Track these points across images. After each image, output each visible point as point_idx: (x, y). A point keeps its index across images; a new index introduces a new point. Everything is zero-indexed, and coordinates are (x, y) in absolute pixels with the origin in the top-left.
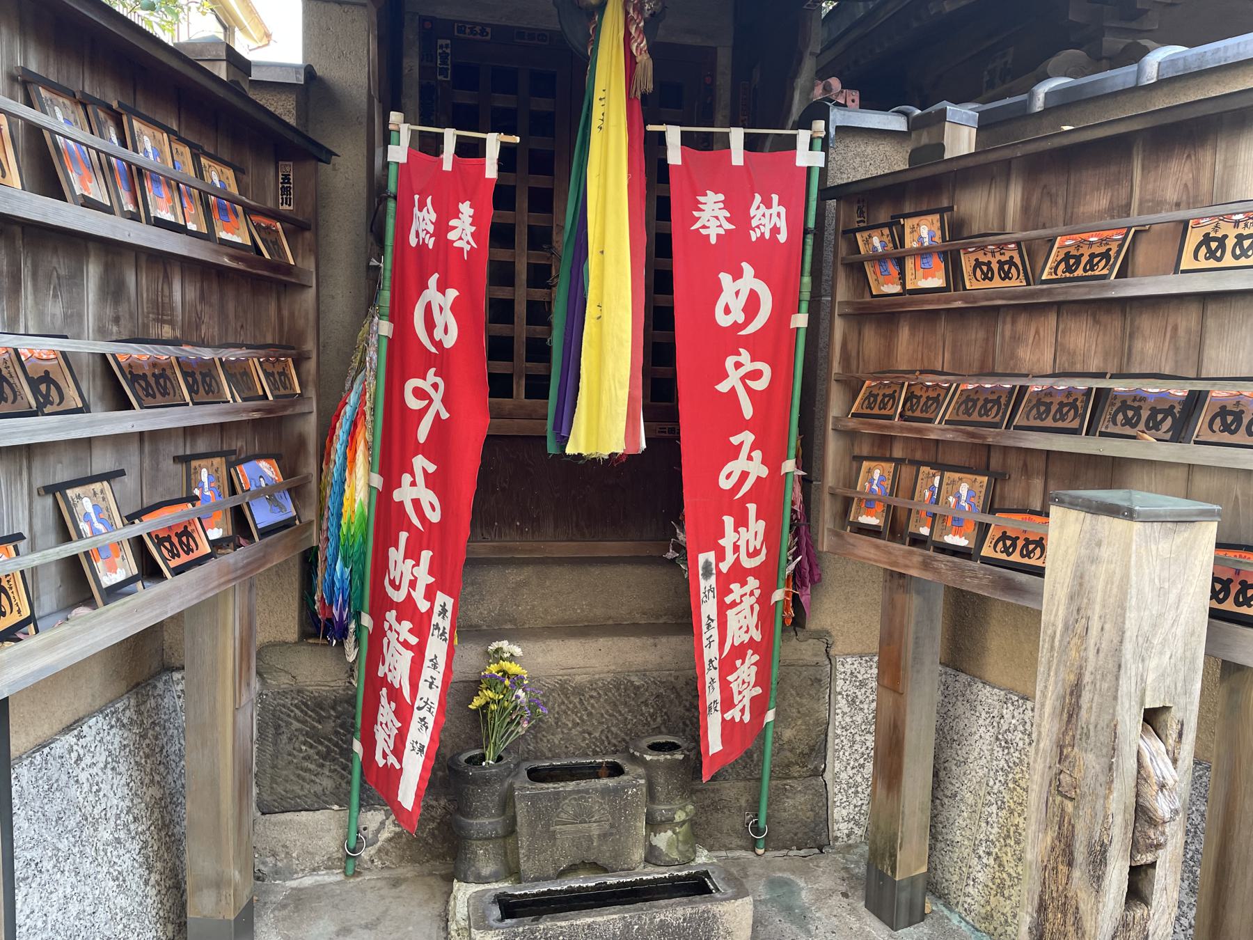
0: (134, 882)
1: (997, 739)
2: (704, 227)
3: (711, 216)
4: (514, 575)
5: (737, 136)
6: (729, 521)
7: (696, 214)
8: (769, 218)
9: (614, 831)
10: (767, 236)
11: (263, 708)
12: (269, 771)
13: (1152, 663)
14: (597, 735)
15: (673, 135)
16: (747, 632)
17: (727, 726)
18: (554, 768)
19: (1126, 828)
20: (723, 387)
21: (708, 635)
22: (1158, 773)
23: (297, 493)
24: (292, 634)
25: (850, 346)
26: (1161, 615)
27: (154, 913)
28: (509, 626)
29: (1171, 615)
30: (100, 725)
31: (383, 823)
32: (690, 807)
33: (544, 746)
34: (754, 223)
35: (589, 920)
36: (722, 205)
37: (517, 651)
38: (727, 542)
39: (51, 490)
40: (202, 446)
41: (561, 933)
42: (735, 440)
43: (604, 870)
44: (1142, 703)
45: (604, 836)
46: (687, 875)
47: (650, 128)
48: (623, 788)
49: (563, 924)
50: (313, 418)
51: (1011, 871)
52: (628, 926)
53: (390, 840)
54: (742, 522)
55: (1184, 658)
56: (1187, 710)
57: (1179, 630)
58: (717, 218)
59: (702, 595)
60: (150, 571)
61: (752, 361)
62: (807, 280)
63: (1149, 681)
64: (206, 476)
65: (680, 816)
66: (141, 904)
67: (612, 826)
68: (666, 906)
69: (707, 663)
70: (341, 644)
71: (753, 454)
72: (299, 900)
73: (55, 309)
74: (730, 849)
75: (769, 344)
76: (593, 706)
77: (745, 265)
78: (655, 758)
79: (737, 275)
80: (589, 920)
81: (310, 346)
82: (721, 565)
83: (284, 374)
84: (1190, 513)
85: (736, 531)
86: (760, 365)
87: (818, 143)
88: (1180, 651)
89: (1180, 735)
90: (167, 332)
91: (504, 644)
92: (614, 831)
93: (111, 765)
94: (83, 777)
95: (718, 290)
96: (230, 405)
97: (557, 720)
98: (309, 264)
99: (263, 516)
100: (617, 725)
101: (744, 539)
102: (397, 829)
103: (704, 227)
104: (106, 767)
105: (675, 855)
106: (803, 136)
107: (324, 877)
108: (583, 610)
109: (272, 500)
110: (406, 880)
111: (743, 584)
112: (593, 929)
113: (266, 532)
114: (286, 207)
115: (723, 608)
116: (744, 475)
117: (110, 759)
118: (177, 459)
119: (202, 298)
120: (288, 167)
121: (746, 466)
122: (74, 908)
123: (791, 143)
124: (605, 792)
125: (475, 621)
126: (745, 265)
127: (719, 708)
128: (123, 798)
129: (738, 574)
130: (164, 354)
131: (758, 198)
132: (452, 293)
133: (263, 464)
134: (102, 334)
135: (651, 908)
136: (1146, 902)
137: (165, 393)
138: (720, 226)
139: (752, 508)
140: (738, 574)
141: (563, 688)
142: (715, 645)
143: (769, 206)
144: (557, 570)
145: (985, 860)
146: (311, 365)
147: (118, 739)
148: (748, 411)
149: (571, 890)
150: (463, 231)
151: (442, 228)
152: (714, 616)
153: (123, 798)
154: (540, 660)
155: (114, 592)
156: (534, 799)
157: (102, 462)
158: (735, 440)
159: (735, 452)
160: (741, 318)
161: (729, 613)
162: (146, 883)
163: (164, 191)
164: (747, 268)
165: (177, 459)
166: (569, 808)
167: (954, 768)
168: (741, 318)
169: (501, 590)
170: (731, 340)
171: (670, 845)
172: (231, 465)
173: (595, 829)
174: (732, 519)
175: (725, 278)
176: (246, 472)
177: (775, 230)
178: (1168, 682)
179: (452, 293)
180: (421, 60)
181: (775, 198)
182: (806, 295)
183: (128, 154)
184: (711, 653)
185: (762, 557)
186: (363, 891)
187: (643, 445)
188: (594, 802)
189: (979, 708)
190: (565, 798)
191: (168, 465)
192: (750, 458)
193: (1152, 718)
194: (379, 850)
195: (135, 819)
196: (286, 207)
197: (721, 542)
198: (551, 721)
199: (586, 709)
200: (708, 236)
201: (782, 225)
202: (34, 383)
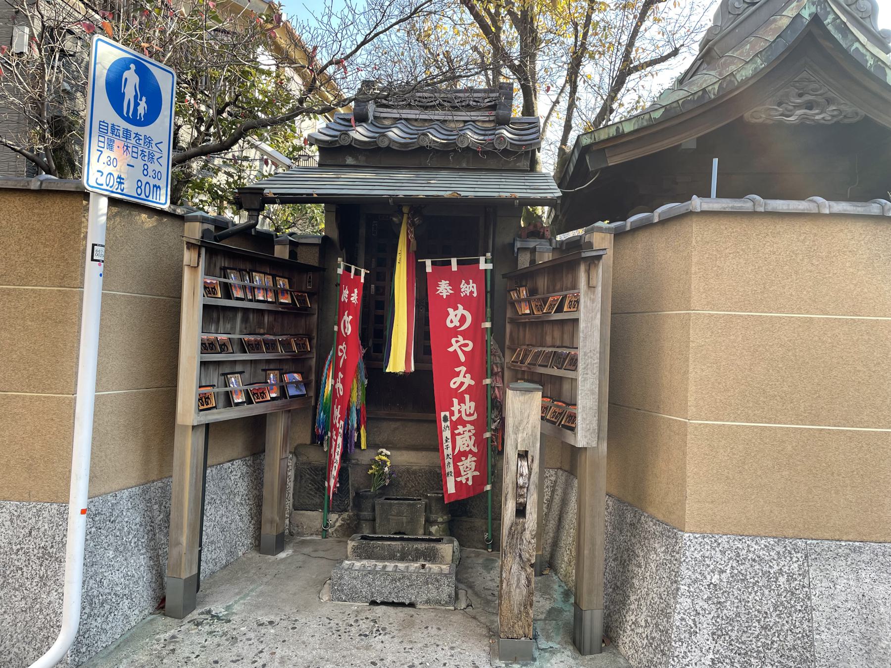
0: (246, 519)
3: (444, 289)
4: (394, 425)
5: (454, 261)
6: (455, 401)
8: (469, 288)
13: (520, 435)
15: (428, 262)
17: (458, 484)
20: (451, 349)
23: (307, 385)
24: (308, 442)
26: (522, 420)
29: (525, 421)
37: (389, 453)
38: (456, 408)
39: (223, 374)
40: (272, 367)
42: (457, 369)
43: (404, 534)
45: (408, 522)
50: (314, 360)
52: (403, 548)
53: (340, 526)
54: (462, 401)
56: (535, 451)
57: (530, 426)
60: (249, 401)
62: (489, 310)
64: (272, 377)
65: (440, 520)
70: (322, 444)
73: (228, 326)
75: (472, 333)
79: (456, 309)
81: (315, 334)
83: (304, 344)
86: (467, 342)
89: (533, 460)
90: (262, 331)
91: (384, 450)
93: (242, 477)
94: (232, 478)
95: (448, 314)
96: (281, 352)
98: (316, 306)
99: (292, 391)
101: (465, 408)
106: (482, 259)
107: (314, 537)
109: (297, 387)
111: (464, 426)
113: (291, 397)
115: (453, 436)
116: (462, 384)
118: (263, 370)
121: (463, 379)
122: (224, 519)
123: (478, 261)
129: (461, 422)
130: (259, 338)
132: (351, 317)
133: (296, 375)
134: (241, 333)
136: (524, 516)
137: (258, 349)
139: (467, 397)
140: (461, 422)
141: (408, 471)
142: (450, 449)
143: (468, 284)
146: (315, 341)
148: (463, 358)
150: (354, 298)
151: (349, 296)
152: (449, 437)
155: (237, 404)
156: (382, 504)
157: (239, 368)
158: (457, 369)
159: (458, 374)
160: (458, 324)
161: (457, 437)
163: (261, 291)
165: (263, 370)
168: (458, 324)
169: (387, 429)
170: (455, 332)
172: (281, 374)
173: (405, 519)
175: (450, 310)
176: (287, 378)
177: (472, 292)
179: (351, 317)
181: (471, 281)
182: (489, 315)
183: (252, 284)
184: (448, 451)
185: (475, 417)
187: (413, 369)
191: (259, 371)
192: (464, 377)
193: (523, 455)
201: (475, 290)
202: (221, 346)
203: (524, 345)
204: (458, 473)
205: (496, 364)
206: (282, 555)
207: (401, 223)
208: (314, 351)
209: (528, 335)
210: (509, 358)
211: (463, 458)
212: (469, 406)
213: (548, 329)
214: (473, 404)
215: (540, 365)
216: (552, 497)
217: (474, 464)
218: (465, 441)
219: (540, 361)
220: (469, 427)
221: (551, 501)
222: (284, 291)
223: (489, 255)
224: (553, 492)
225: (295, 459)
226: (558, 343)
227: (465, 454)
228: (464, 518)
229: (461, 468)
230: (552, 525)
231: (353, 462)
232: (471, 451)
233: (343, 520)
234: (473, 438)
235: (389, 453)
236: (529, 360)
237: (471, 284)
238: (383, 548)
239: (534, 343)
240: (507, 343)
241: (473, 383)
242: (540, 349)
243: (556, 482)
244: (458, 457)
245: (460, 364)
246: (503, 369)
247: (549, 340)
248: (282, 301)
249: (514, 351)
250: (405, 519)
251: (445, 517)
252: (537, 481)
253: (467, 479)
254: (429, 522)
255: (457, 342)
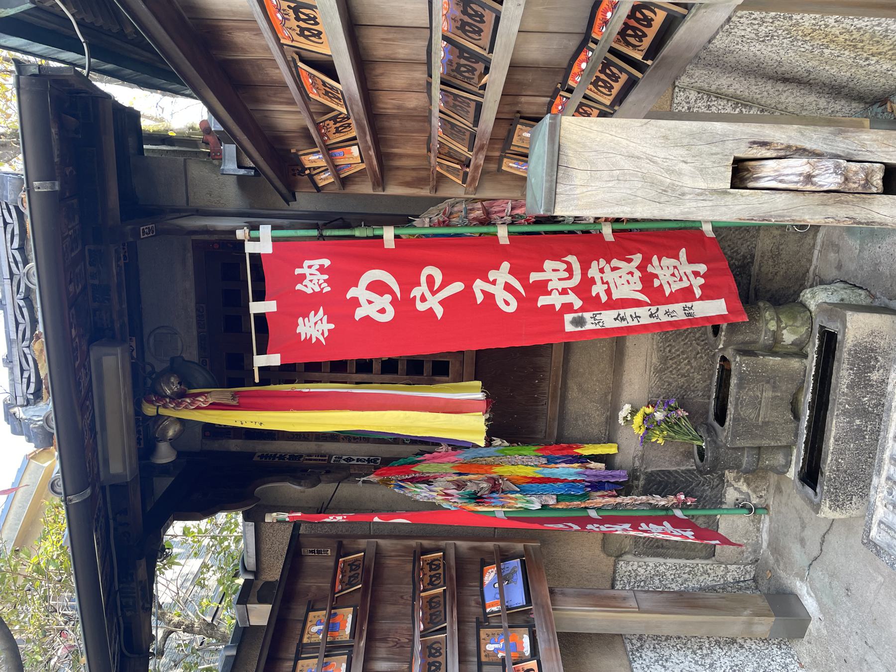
1: (763, 41)
2: (323, 334)
3: (314, 327)
4: (573, 393)
5: (256, 308)
6: (543, 301)
7: (314, 340)
9: (772, 381)
10: (326, 277)
11: (644, 554)
12: (686, 552)
13: (688, 183)
14: (699, 348)
15: (260, 361)
16: (632, 273)
17: (709, 293)
18: (717, 398)
19: (841, 202)
20: (439, 312)
21: (629, 319)
22: (796, 179)
25: (408, 179)
26: (644, 178)
27: (762, 644)
28: (610, 397)
30: (638, 666)
31: (736, 489)
32: (767, 315)
33: (701, 385)
34: (317, 289)
35: (832, 440)
36: (306, 319)
37: (626, 409)
38: (556, 300)
40: (472, 646)
41: (836, 460)
42: (480, 298)
44: (724, 192)
45: (775, 388)
46: (820, 340)
47: (257, 380)
48: (740, 373)
49: (829, 459)
50: (458, 543)
51: (887, 48)
52: (845, 413)
53: (748, 485)
54: (542, 288)
55: (689, 146)
56: (736, 137)
57: (662, 153)
58: (316, 323)
59: (598, 327)
61: (420, 285)
62: (357, 233)
63: (703, 185)
65: (772, 326)
66: (754, 654)
67: (768, 382)
68: (837, 382)
69: (654, 320)
71: (491, 280)
72: (775, 547)
74: (814, 244)
76: (677, 350)
77: (348, 296)
78: (722, 342)
79: (356, 303)
80: (832, 440)
81: (413, 543)
82: (576, 308)
84: (551, 152)
85: (549, 293)
86: (423, 279)
87: (254, 234)
88: (682, 152)
89: (764, 144)
92: (772, 381)
95: (367, 318)
97: (683, 376)
98: (363, 543)
100: (695, 333)
102: (742, 480)
103: (323, 334)
104: (664, 667)
105: (803, 330)
106: (250, 248)
108: (604, 346)
110: (779, 483)
111: (593, 281)
112: (840, 438)
113: (529, 601)
114: (329, 552)
115: (613, 304)
116: (508, 287)
117: (660, 662)
119: (384, 640)
120: (305, 551)
121: (499, 286)
124: (740, 386)
125: (603, 419)
126: (348, 296)
127: (689, 304)
128: (686, 656)
129: (584, 289)
131: (299, 287)
135: (835, 392)
138: (321, 320)
139: (534, 277)
140: (584, 289)
141: (659, 371)
142: (640, 311)
143: (303, 277)
144: (573, 364)
145: (872, 62)
146: (426, 543)
147: (649, 653)
148: (457, 287)
149: (808, 428)
152: (614, 313)
153: (686, 656)
154: (637, 387)
158: (480, 298)
160: (388, 297)
162: (742, 647)
164: (351, 293)
166: (748, 413)
167: (783, 69)
168: (388, 297)
169: (583, 406)
170: (404, 305)
171: (794, 333)
173: (768, 394)
174: (541, 298)
175: (359, 314)
176: (493, 608)
177: (321, 269)
178: (708, 164)
180: (230, 438)
181: (298, 271)
182: (368, 232)
184: (644, 316)
185: (572, 259)
186: (779, 512)
188: (746, 395)
189: (732, 48)
190: (739, 414)
192: (494, 283)
193: (741, 173)
194: (755, 492)
195: (701, 648)
196: (329, 552)
197: (558, 308)
198: (683, 380)
199: (679, 355)
200: (329, 330)
201: (317, 263)
203: (428, 159)
204: (686, 294)
205: (469, 211)
206: (810, 604)
207: (181, 421)
208: (442, 543)
209: (407, 151)
210: (456, 189)
211: (656, 283)
212: (552, 272)
213: (388, 103)
214: (548, 264)
215: (476, 122)
216: (728, 98)
217: (666, 261)
218: (620, 279)
219: (466, 123)
220: (593, 272)
221: (737, 100)
222: (331, 626)
223: (240, 234)
224: (719, 95)
225: (628, 557)
226: (420, 75)
227: (647, 279)
228: (755, 269)
229: (676, 287)
230: (790, 97)
231: (637, 464)
232: (642, 268)
233: (737, 479)
234: (615, 262)
235: (626, 409)
236: (462, 149)
237: (305, 270)
238: (840, 452)
239: (423, 137)
240: (425, 192)
241: (506, 266)
242: (436, 122)
243: (700, 90)
244: (654, 294)
245: (468, 292)
246: (475, 200)
247: (414, 101)
248: (348, 630)
249: (441, 178)
250: (768, 394)
251: (767, 315)
252: (826, 131)
253: (696, 274)
254: (774, 348)
255: (423, 299)
